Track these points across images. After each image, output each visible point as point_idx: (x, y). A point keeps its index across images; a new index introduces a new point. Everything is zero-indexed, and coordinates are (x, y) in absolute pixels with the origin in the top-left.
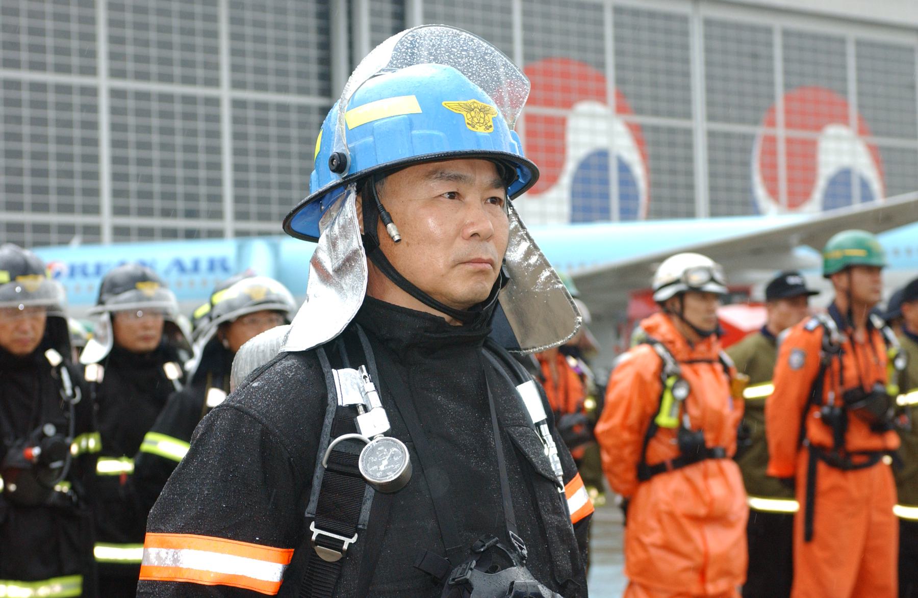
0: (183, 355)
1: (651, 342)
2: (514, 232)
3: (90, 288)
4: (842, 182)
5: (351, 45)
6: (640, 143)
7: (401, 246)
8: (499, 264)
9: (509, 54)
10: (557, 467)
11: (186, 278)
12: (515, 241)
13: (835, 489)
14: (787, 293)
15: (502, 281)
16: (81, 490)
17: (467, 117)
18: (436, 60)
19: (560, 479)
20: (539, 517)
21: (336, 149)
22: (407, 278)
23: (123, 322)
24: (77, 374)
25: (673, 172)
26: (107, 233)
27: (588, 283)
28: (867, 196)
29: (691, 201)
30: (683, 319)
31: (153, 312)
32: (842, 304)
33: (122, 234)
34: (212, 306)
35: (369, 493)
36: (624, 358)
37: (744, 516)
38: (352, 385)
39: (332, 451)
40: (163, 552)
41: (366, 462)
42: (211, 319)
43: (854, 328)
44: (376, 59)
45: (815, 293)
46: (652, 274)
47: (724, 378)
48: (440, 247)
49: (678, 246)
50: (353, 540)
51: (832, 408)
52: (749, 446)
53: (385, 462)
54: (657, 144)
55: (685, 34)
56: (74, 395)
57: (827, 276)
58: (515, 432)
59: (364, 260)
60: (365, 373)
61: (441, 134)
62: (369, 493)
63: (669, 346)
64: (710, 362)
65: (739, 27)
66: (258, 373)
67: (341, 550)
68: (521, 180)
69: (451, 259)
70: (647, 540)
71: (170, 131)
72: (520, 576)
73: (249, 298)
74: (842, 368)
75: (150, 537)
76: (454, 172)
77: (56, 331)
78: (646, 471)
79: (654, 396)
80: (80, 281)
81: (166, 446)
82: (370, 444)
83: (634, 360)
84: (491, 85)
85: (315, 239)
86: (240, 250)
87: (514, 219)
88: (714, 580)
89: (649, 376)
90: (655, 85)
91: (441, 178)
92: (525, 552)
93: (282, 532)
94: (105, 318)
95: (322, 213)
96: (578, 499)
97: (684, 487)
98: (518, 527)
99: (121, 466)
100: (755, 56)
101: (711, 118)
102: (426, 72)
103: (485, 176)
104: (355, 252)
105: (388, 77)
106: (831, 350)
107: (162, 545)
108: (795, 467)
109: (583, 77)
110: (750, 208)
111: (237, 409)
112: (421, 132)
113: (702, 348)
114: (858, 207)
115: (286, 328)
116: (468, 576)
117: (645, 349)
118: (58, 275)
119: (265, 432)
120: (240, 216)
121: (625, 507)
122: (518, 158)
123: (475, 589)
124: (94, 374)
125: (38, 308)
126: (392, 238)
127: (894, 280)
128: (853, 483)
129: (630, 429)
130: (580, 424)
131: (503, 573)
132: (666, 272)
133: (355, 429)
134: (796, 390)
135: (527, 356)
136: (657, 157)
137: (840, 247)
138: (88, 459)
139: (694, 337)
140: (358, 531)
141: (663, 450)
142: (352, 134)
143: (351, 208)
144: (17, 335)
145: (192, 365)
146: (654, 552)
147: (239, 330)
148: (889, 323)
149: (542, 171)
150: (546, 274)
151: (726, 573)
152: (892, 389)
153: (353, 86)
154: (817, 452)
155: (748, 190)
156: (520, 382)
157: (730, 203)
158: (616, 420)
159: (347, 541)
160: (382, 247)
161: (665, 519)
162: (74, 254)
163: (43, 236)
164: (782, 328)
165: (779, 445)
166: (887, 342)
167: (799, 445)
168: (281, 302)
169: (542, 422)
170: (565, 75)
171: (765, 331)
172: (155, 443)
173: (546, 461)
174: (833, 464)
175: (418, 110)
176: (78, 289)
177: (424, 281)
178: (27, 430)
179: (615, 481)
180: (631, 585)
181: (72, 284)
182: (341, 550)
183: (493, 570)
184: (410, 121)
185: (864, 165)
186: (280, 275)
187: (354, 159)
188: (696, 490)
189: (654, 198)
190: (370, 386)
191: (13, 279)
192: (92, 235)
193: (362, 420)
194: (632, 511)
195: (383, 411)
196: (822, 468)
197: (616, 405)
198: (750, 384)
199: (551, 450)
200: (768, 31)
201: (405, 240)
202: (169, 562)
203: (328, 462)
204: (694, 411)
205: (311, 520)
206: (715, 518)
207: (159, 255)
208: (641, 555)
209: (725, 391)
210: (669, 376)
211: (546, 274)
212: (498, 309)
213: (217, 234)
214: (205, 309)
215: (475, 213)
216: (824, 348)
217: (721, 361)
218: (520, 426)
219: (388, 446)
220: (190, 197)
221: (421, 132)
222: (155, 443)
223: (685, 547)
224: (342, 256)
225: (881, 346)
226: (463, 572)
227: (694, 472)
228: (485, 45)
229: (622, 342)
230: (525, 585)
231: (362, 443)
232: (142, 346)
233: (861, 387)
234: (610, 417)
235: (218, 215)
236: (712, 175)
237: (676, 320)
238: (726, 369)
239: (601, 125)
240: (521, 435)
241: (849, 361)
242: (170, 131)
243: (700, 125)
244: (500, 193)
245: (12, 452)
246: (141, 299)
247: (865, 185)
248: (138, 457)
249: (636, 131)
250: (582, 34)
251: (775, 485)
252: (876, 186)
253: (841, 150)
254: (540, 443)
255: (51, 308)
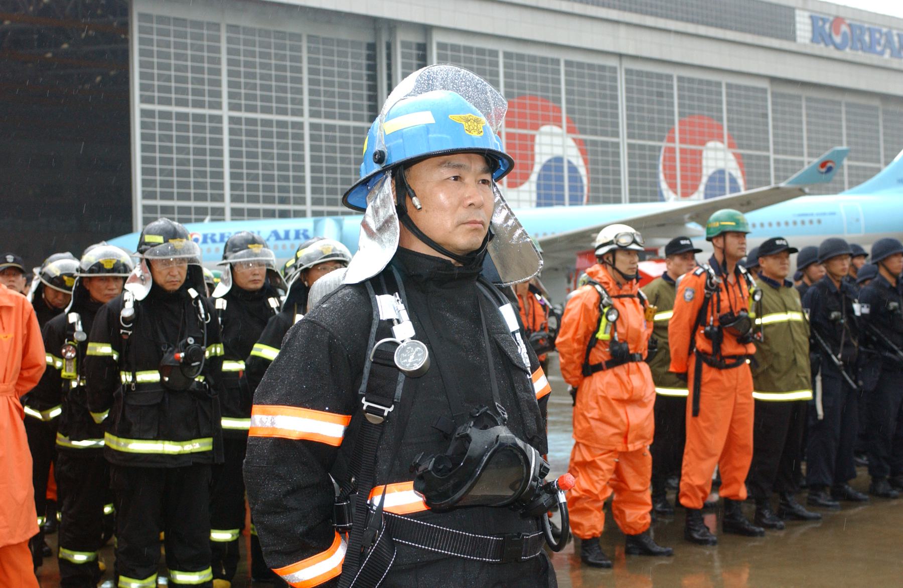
0: (281, 292)
1: (593, 284)
2: (498, 203)
3: (217, 250)
4: (719, 175)
5: (390, 77)
6: (583, 152)
7: (422, 212)
8: (488, 225)
9: (495, 84)
10: (527, 361)
11: (280, 243)
12: (498, 211)
13: (713, 381)
14: (680, 250)
15: (490, 236)
16: (212, 381)
17: (466, 125)
18: (444, 88)
19: (529, 369)
20: (515, 394)
21: (377, 148)
22: (426, 234)
23: (238, 270)
24: (210, 306)
25: (606, 172)
26: (228, 213)
27: (549, 245)
28: (735, 188)
29: (618, 191)
30: (614, 268)
31: (260, 264)
32: (719, 258)
33: (238, 214)
34: (297, 259)
35: (401, 378)
36: (574, 294)
37: (653, 398)
38: (389, 306)
39: (377, 350)
40: (264, 417)
41: (399, 356)
42: (296, 268)
43: (727, 275)
44: (405, 86)
45: (699, 251)
46: (594, 240)
47: (641, 307)
48: (449, 214)
49: (611, 221)
50: (391, 409)
51: (712, 327)
52: (656, 352)
53: (412, 357)
54: (595, 153)
55: (615, 79)
56: (207, 318)
57: (709, 239)
58: (499, 338)
59: (397, 222)
60: (398, 298)
61: (448, 137)
62: (401, 378)
63: (606, 286)
64: (632, 296)
65: (649, 75)
66: (326, 298)
67: (382, 416)
68: (502, 168)
69: (455, 221)
70: (589, 415)
71: (270, 145)
72: (503, 432)
73: (322, 253)
74: (719, 300)
75: (255, 408)
76: (456, 163)
77: (194, 274)
78: (589, 369)
79: (594, 320)
80: (210, 245)
81: (266, 352)
82: (402, 345)
83: (582, 294)
84: (482, 105)
85: (363, 210)
86: (316, 223)
87: (497, 195)
88: (632, 442)
89: (591, 307)
90: (594, 114)
91: (449, 166)
92: (506, 416)
93: (344, 404)
94: (228, 267)
95: (369, 191)
96: (540, 384)
97: (614, 380)
98: (501, 400)
99: (238, 366)
100: (660, 94)
101: (630, 136)
102: (439, 96)
103: (478, 165)
104: (391, 217)
105: (411, 99)
106: (712, 288)
107: (264, 413)
108: (687, 367)
109: (546, 108)
110: (657, 196)
111: (313, 322)
112: (435, 135)
113: (627, 287)
114: (728, 196)
115: (345, 269)
116: (468, 432)
117: (588, 288)
118: (196, 240)
119: (332, 337)
120: (315, 202)
121: (574, 393)
122: (500, 153)
123: (473, 440)
124: (221, 304)
125: (183, 259)
126: (416, 207)
127: (754, 242)
128: (727, 377)
129: (578, 341)
130: (543, 339)
131: (492, 430)
132: (601, 238)
133: (391, 335)
134: (688, 315)
135: (509, 287)
136: (595, 162)
137: (718, 220)
138: (216, 361)
139: (622, 280)
140: (394, 403)
141: (600, 355)
142: (388, 138)
143: (388, 187)
144: (169, 278)
145: (284, 299)
146: (593, 422)
147: (314, 274)
148: (749, 271)
149: (517, 161)
150: (519, 232)
151: (641, 437)
152: (752, 315)
153: (389, 104)
154: (702, 356)
155: (656, 184)
156: (501, 304)
157: (644, 193)
158: (569, 335)
159: (387, 410)
160: (409, 213)
161: (601, 401)
162: (207, 227)
163: (186, 215)
164: (678, 276)
165: (676, 351)
166: (749, 283)
167: (690, 352)
168: (343, 256)
169: (517, 331)
170: (534, 107)
171: (665, 276)
172: (260, 350)
173: (519, 357)
174: (712, 365)
175: (432, 120)
176: (209, 250)
177: (437, 235)
178: (176, 341)
179: (568, 376)
180: (577, 444)
181: (205, 246)
182: (382, 416)
183: (485, 428)
184: (427, 128)
185: (733, 168)
186: (342, 240)
187: (390, 154)
188: (622, 382)
189: (592, 190)
190: (402, 307)
191: (166, 241)
192: (218, 215)
193: (396, 329)
194: (578, 395)
195: (410, 323)
196: (705, 366)
197: (569, 325)
198: (659, 311)
199: (522, 350)
200: (669, 77)
201: (424, 208)
202: (268, 424)
203: (374, 357)
204: (621, 329)
205: (362, 396)
206: (634, 401)
207: (262, 228)
208: (585, 425)
209: (642, 316)
210: (604, 307)
211: (519, 232)
212: (487, 256)
213: (301, 214)
214: (293, 261)
215: (471, 190)
216: (707, 288)
217: (639, 295)
218: (502, 333)
219: (414, 346)
220: (282, 189)
221: (435, 135)
222: (260, 350)
223: (615, 420)
224: (382, 220)
225: (745, 286)
226: (465, 430)
227: (620, 370)
228: (477, 78)
229: (572, 285)
230: (506, 438)
231: (397, 344)
232: (252, 286)
233: (731, 313)
234: (565, 333)
235: (302, 201)
236: (631, 174)
237: (609, 268)
238: (642, 301)
239: (557, 141)
240: (503, 339)
241: (724, 296)
242: (270, 145)
243: (623, 141)
244: (488, 177)
245: (166, 355)
246: (250, 255)
247: (733, 180)
248: (248, 359)
249: (580, 143)
250: (546, 80)
251: (674, 378)
252: (741, 182)
253: (717, 157)
254: (515, 345)
255: (191, 260)
